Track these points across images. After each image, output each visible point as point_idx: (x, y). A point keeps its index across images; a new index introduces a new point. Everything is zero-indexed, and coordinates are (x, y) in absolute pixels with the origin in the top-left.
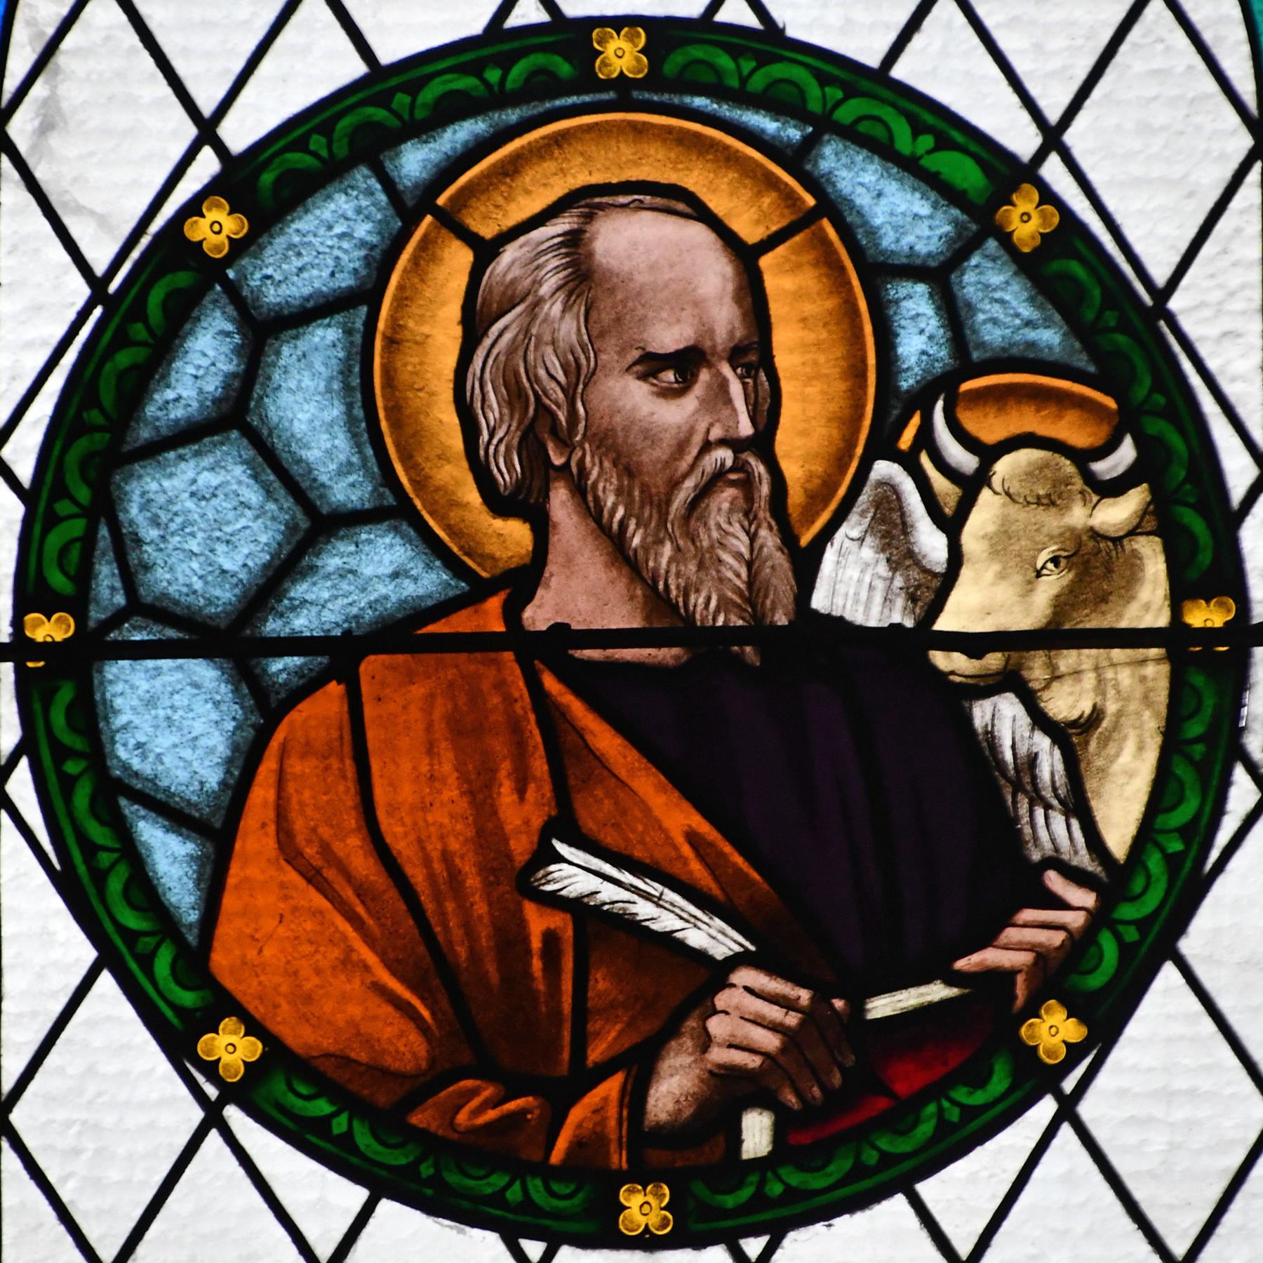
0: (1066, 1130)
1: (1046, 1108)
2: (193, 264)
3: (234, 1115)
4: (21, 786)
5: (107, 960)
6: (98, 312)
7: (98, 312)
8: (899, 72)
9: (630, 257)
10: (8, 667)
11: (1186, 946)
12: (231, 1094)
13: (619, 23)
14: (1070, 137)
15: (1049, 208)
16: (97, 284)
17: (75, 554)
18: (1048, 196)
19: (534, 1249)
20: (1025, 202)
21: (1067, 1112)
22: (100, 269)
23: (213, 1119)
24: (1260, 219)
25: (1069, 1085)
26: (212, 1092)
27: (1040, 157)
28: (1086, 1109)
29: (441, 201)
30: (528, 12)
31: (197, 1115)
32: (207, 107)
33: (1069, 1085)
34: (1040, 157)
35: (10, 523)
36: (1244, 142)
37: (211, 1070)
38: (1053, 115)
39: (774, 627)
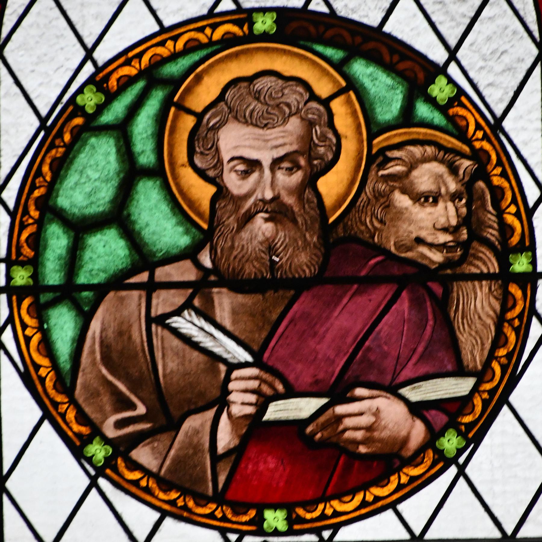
0: (462, 480)
1: (453, 470)
2: (105, 85)
3: (102, 482)
4: (7, 337)
5: (46, 415)
6: (42, 134)
7: (42, 134)
8: (387, 29)
9: (364, 65)
10: (4, 297)
11: (512, 399)
12: (100, 472)
13: (264, 10)
14: (459, 55)
15: (450, 85)
16: (43, 120)
17: (510, 303)
18: (451, 81)
19: (233, 537)
20: (441, 81)
21: (461, 472)
22: (44, 112)
23: (93, 484)
24: (1, 244)
25: (461, 460)
26: (93, 473)
27: (447, 63)
28: (468, 470)
29: (176, 99)
30: (227, 5)
31: (86, 482)
32: (89, 42)
33: (461, 460)
34: (447, 63)
35: (104, 41)
36: (535, 51)
37: (90, 460)
38: (453, 42)
39: (502, 282)
